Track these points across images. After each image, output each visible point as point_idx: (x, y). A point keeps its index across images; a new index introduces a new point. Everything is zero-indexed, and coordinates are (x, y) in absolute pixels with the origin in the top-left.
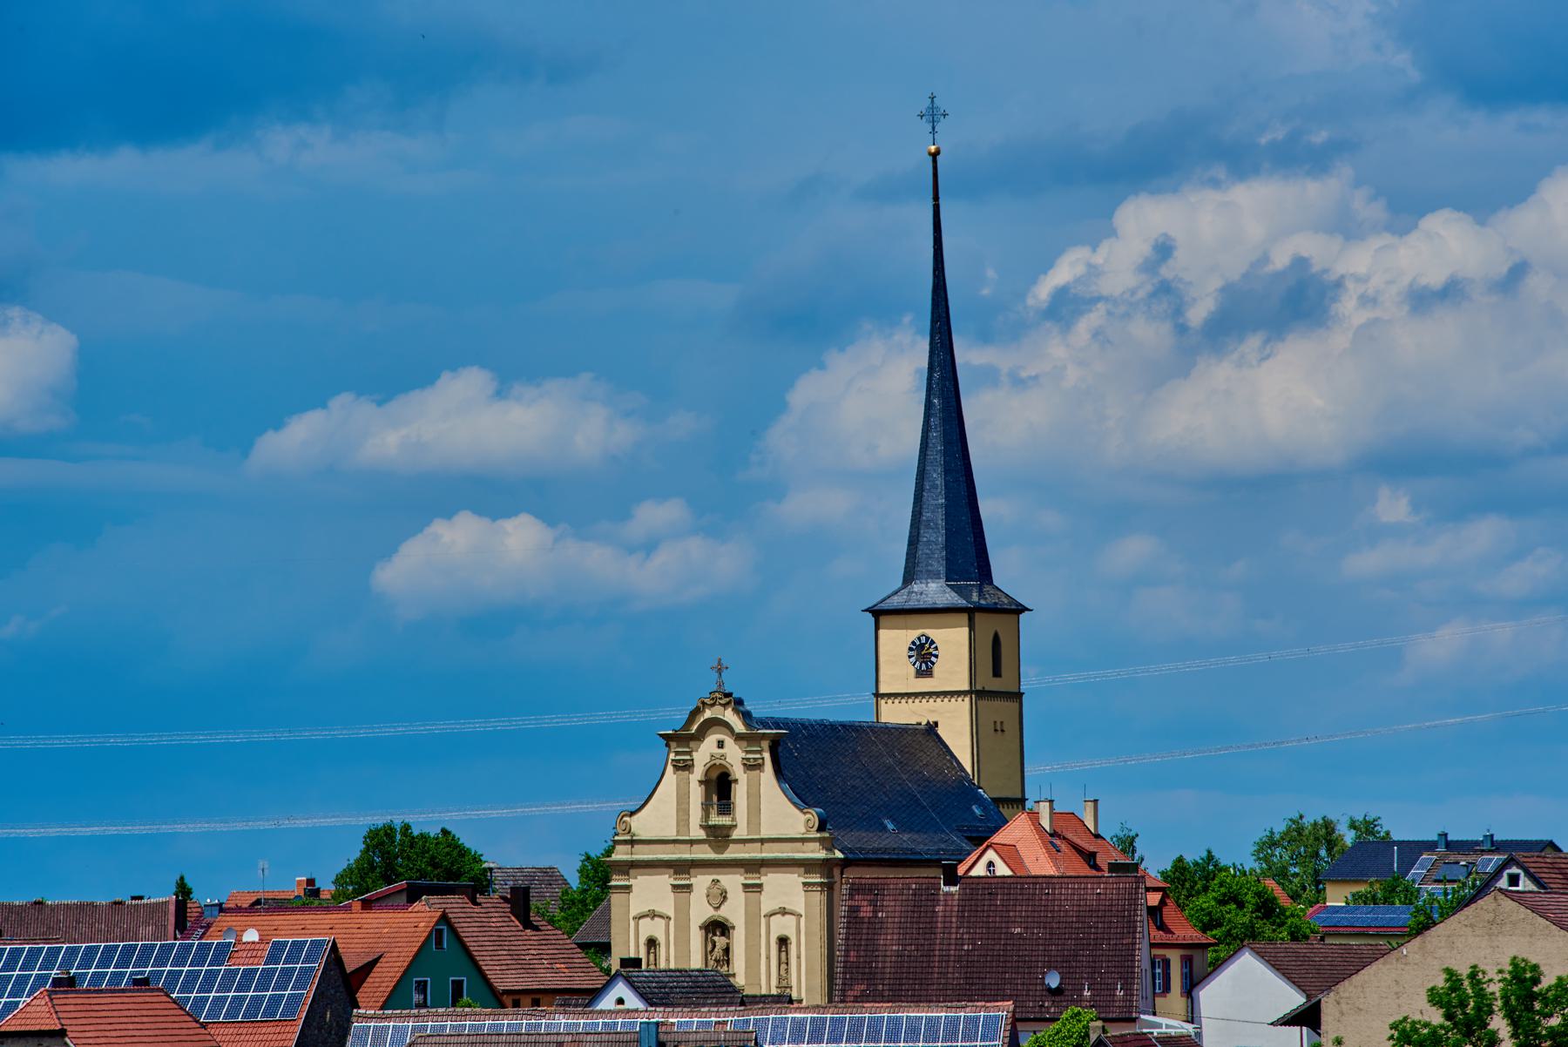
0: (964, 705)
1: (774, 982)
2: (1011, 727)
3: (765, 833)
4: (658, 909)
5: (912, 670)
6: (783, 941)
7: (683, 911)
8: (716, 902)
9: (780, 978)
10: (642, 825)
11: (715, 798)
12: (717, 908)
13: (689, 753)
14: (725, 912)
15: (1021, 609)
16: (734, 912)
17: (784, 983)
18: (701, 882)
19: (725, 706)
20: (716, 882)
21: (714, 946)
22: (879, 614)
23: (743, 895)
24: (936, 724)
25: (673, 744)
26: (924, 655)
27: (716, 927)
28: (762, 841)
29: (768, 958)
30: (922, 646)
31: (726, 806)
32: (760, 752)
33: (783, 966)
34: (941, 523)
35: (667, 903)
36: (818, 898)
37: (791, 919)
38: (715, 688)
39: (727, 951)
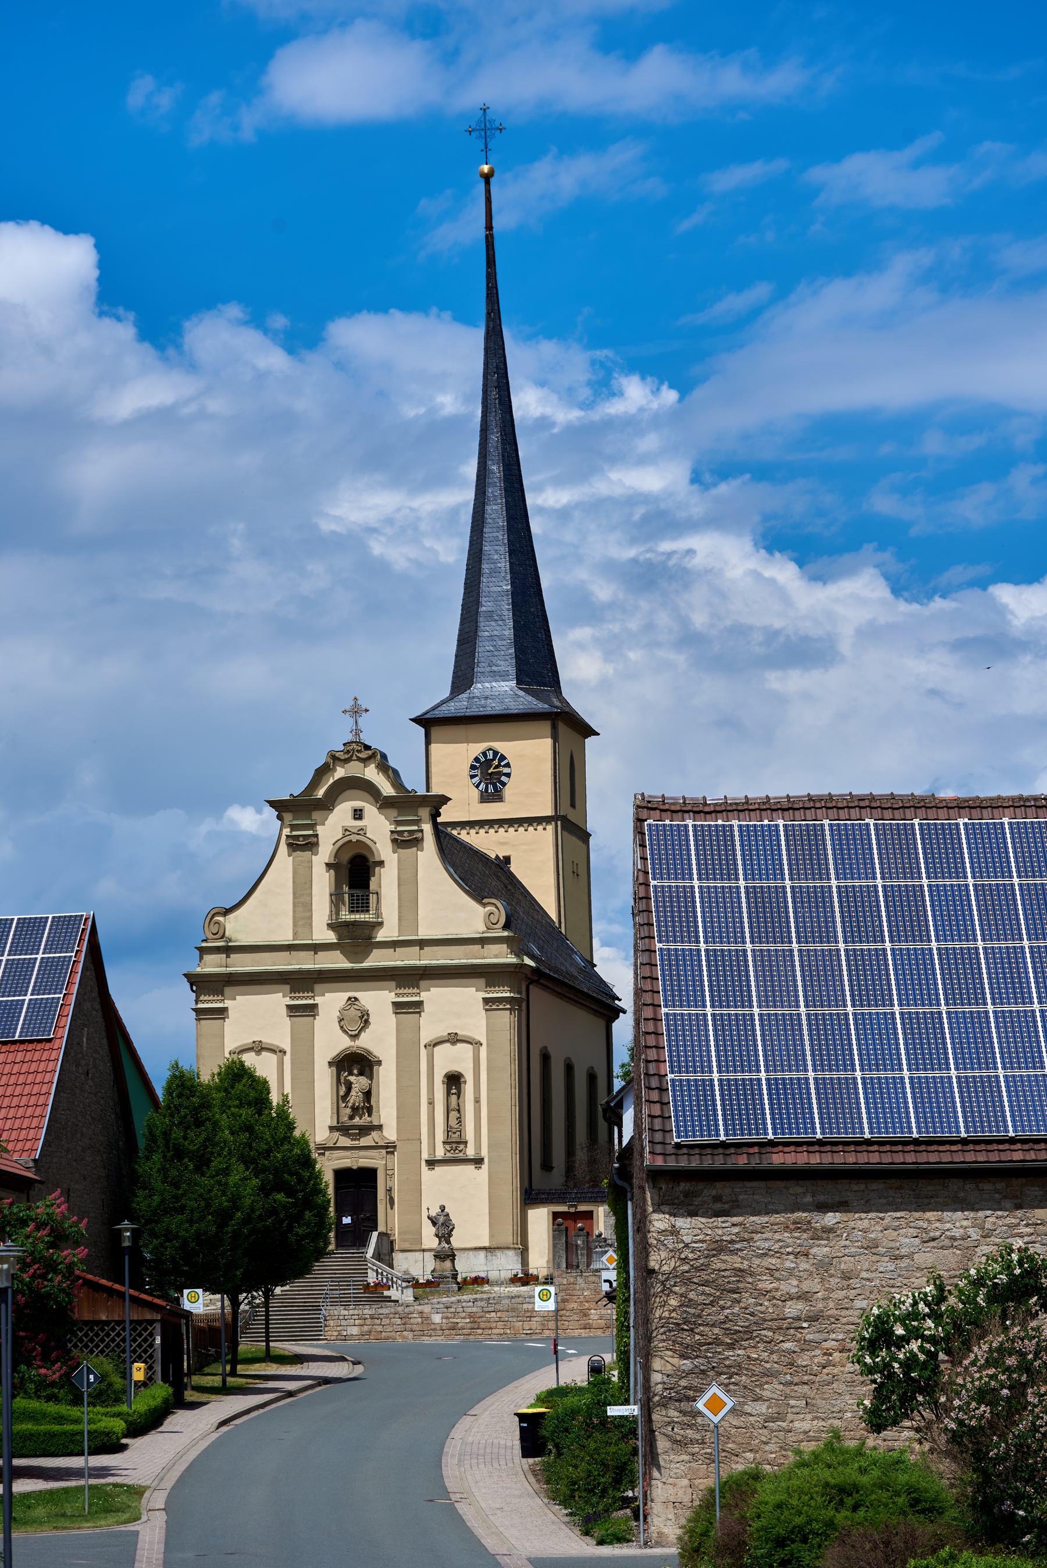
0: (546, 835)
1: (440, 1136)
4: (267, 1040)
5: (475, 793)
6: (454, 1080)
7: (304, 1045)
9: (448, 1130)
10: (240, 927)
11: (346, 889)
12: (355, 1037)
13: (312, 826)
14: (366, 1042)
15: (588, 731)
16: (381, 1039)
17: (455, 1137)
18: (331, 1002)
19: (365, 761)
21: (349, 1089)
22: (428, 722)
23: (393, 1018)
25: (288, 817)
26: (491, 775)
28: (422, 943)
29: (431, 1103)
30: (488, 763)
32: (417, 822)
33: (454, 1115)
34: (508, 615)
35: (279, 1031)
36: (506, 1019)
38: (350, 737)
39: (368, 1095)
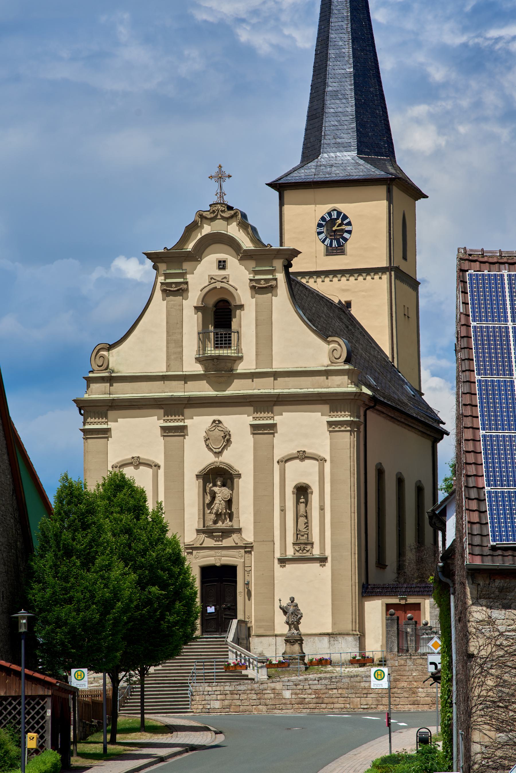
0: (382, 283)
1: (290, 538)
2: (412, 315)
3: (277, 366)
4: (144, 456)
5: (321, 248)
7: (175, 460)
10: (121, 361)
12: (218, 454)
13: (183, 275)
14: (228, 458)
16: (240, 456)
17: (303, 539)
18: (198, 424)
20: (217, 423)
21: (213, 498)
22: (281, 187)
23: (250, 439)
24: (349, 304)
25: (163, 267)
27: (218, 476)
28: (276, 375)
29: (283, 510)
30: (333, 221)
31: (223, 341)
32: (272, 272)
33: (302, 520)
35: (156, 450)
36: (347, 440)
37: (311, 465)
39: (229, 503)
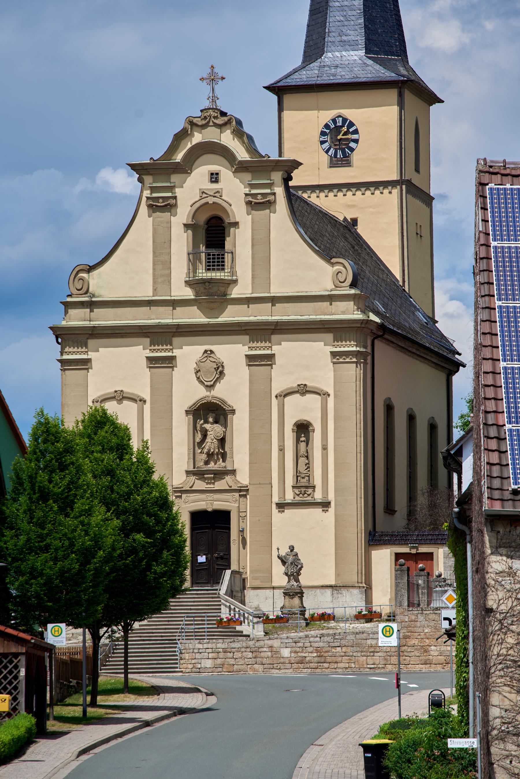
1: (290, 481)
2: (425, 233)
4: (128, 389)
5: (325, 159)
7: (163, 394)
8: (209, 379)
9: (297, 476)
10: (103, 283)
12: (210, 387)
13: (171, 189)
14: (221, 392)
16: (235, 390)
17: (304, 482)
18: (188, 354)
21: (205, 436)
24: (355, 221)
25: (148, 180)
26: (340, 140)
27: (208, 412)
28: (274, 300)
29: (282, 449)
32: (270, 186)
35: (141, 382)
36: (352, 372)
38: (207, 104)
39: (222, 441)
